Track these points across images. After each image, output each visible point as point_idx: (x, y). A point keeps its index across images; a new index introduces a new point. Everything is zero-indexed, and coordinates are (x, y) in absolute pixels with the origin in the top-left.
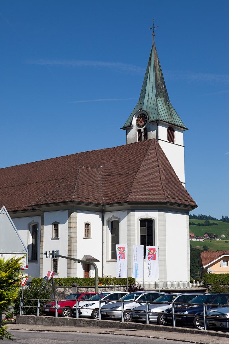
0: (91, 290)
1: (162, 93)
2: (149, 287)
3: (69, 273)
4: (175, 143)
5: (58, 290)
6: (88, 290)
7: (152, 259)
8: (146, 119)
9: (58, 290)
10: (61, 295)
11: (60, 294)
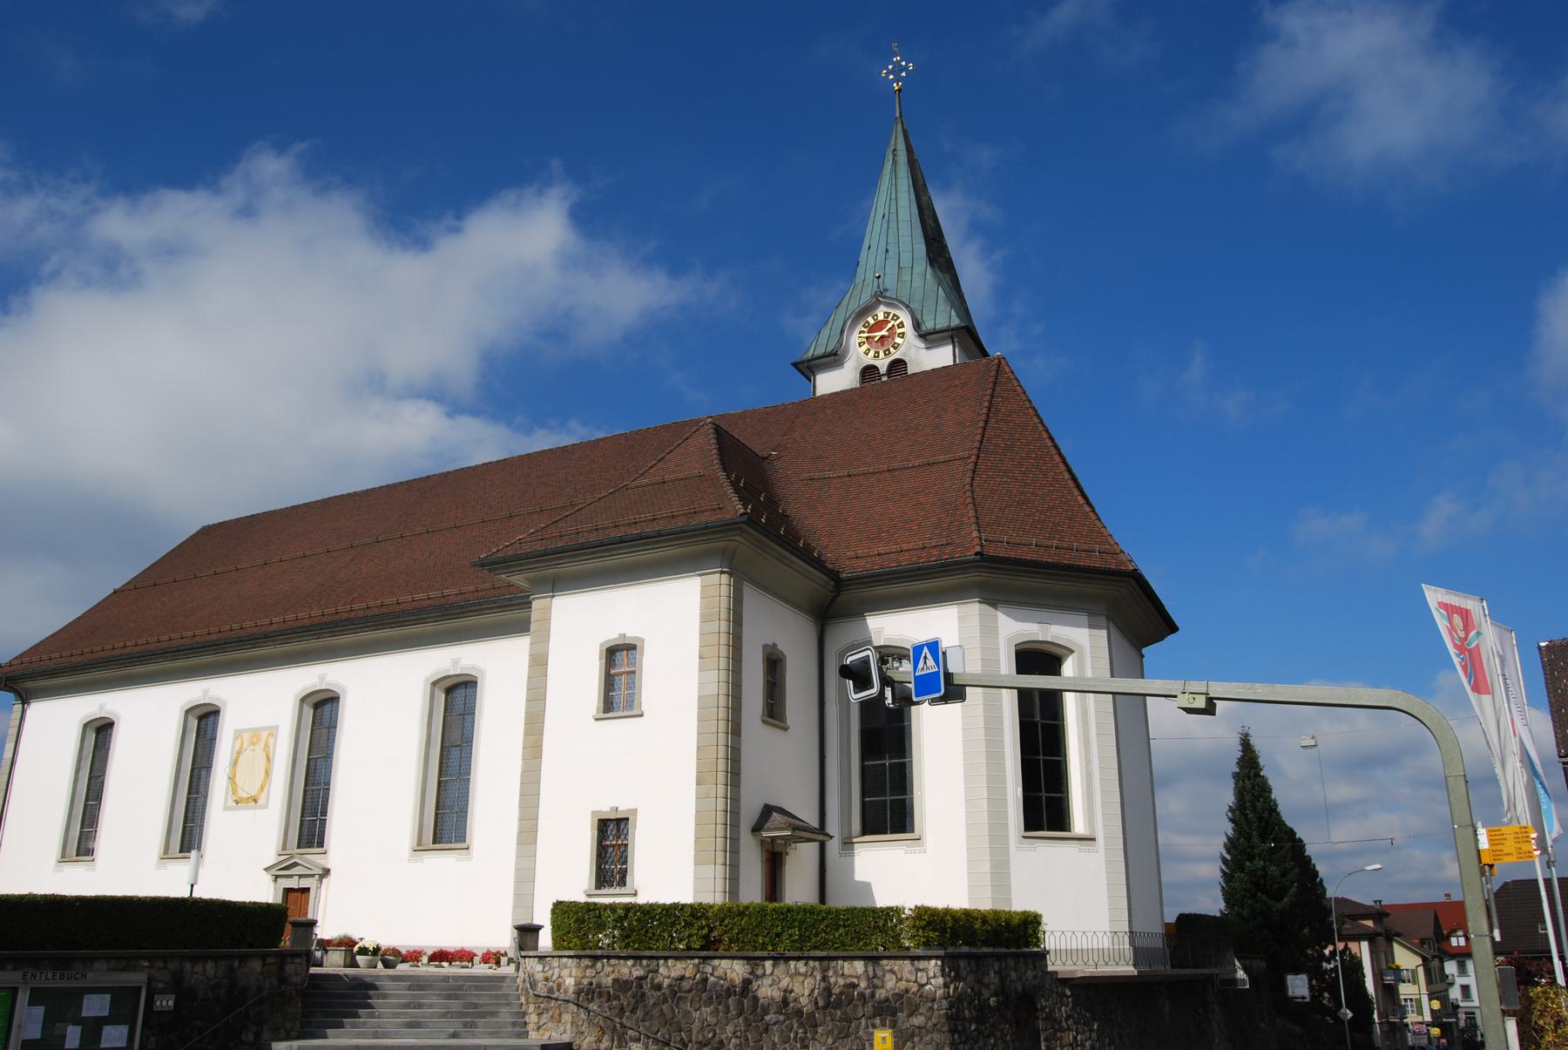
0: (892, 971)
6: (879, 973)
9: (714, 968)
11: (729, 992)
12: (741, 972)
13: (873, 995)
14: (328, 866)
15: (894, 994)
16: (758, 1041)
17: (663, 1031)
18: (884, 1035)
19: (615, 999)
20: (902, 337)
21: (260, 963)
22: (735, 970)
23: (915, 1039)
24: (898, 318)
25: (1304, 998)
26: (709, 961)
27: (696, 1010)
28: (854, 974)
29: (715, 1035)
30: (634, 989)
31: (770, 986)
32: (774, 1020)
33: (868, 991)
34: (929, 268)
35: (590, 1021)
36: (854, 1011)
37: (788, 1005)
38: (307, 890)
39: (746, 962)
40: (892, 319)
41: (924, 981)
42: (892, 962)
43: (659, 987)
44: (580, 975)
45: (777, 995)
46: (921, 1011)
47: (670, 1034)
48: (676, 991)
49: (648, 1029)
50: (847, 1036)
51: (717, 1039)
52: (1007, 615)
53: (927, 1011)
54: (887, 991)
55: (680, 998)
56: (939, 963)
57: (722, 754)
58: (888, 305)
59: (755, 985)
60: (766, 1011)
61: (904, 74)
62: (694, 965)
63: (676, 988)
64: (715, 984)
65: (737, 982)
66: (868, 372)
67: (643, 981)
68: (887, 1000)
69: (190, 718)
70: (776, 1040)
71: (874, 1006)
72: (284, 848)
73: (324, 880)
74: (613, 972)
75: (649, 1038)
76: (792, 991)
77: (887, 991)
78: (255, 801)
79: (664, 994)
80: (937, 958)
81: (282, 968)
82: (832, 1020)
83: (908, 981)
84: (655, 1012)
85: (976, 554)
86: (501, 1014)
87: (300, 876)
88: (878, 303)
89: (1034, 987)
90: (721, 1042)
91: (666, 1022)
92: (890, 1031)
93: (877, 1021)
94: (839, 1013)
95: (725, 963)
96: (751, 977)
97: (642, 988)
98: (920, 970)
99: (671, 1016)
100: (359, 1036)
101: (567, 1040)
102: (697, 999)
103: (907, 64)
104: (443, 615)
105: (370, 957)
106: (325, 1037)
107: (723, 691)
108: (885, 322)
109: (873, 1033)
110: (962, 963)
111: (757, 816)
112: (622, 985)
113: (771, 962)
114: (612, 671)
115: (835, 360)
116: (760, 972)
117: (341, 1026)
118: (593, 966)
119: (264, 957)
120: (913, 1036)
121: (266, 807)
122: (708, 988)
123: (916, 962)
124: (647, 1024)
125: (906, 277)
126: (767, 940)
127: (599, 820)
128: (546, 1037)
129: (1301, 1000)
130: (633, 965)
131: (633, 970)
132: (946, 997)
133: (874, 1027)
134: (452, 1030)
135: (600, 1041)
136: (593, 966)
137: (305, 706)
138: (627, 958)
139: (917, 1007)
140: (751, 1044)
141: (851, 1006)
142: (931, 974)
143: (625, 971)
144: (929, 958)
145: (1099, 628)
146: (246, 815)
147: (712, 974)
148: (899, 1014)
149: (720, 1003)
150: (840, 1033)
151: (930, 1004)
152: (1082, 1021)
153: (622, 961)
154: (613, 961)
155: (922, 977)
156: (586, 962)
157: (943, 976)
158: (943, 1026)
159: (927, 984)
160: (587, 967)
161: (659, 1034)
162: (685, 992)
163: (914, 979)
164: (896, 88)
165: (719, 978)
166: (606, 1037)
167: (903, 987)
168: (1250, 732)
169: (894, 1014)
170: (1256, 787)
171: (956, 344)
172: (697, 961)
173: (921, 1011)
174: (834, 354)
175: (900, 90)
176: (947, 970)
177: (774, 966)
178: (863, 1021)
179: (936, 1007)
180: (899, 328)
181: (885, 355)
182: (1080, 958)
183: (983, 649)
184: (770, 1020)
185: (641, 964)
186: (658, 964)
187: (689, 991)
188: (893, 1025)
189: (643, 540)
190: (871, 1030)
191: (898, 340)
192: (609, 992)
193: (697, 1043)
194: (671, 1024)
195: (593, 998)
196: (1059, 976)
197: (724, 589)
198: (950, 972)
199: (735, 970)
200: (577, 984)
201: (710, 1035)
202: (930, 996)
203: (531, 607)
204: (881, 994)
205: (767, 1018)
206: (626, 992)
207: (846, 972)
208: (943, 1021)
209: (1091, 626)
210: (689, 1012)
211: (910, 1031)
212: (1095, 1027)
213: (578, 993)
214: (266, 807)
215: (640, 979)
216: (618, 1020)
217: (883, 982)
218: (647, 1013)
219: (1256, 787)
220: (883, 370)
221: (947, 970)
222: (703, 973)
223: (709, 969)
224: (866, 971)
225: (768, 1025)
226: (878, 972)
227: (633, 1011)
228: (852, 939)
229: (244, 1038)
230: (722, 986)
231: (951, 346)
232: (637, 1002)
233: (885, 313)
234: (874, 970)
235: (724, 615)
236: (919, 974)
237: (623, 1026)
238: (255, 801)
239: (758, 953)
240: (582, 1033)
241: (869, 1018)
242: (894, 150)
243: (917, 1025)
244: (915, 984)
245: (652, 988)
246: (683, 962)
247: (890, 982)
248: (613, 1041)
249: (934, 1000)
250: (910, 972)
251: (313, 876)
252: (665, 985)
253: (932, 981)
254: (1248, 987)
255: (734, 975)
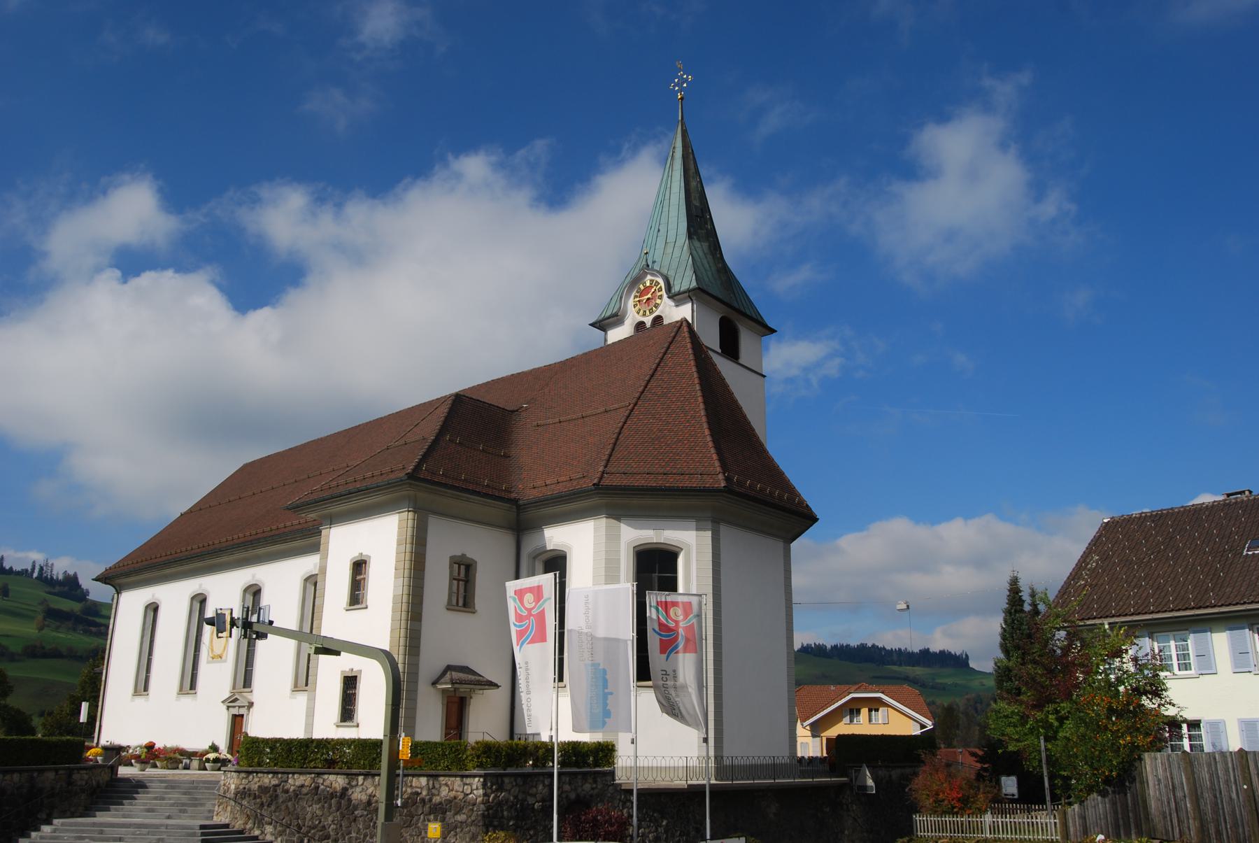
0: (446, 785)
1: (703, 231)
2: (663, 776)
3: (309, 725)
4: (741, 361)
5: (324, 780)
6: (437, 786)
7: (532, 642)
8: (659, 294)
9: (324, 780)
10: (333, 801)
11: (333, 795)
12: (341, 783)
13: (430, 800)
14: (253, 701)
15: (446, 800)
16: (348, 827)
17: (287, 818)
18: (434, 826)
19: (258, 798)
20: (661, 299)
21: (54, 773)
22: (338, 782)
23: (458, 830)
24: (659, 284)
25: (1013, 795)
26: (321, 776)
27: (309, 806)
28: (419, 786)
29: (320, 823)
30: (271, 792)
31: (360, 792)
32: (360, 814)
33: (428, 797)
34: (687, 240)
35: (242, 811)
36: (416, 810)
37: (371, 804)
38: (242, 716)
39: (345, 776)
40: (655, 285)
41: (469, 791)
42: (447, 778)
43: (287, 791)
44: (239, 783)
45: (364, 798)
46: (464, 812)
47: (291, 821)
48: (297, 794)
49: (277, 817)
50: (409, 826)
51: (321, 824)
52: (629, 525)
53: (468, 812)
54: (441, 798)
55: (301, 798)
56: (482, 780)
57: (403, 634)
58: (652, 275)
59: (350, 792)
60: (356, 808)
61: (685, 85)
62: (311, 778)
63: (298, 792)
64: (323, 790)
65: (338, 789)
66: (640, 326)
67: (277, 788)
68: (440, 803)
69: (195, 602)
70: (361, 827)
71: (430, 807)
72: (234, 687)
73: (251, 709)
74: (259, 781)
75: (277, 822)
76: (375, 796)
77: (441, 798)
78: (221, 657)
79: (289, 796)
80: (480, 776)
81: (70, 776)
82: (400, 815)
83: (457, 791)
84: (283, 807)
85: (594, 485)
86: (207, 805)
87: (239, 707)
88: (646, 274)
89: (591, 796)
90: (324, 827)
91: (289, 813)
92: (440, 824)
93: (432, 817)
94: (405, 811)
95: (332, 777)
96: (348, 786)
97: (276, 791)
98: (467, 784)
99: (293, 809)
100: (124, 816)
101: (227, 822)
102: (311, 799)
103: (687, 77)
104: (303, 536)
105: (212, 764)
106: (95, 816)
107: (406, 592)
108: (651, 287)
109: (427, 825)
110: (506, 780)
111: (440, 674)
112: (264, 789)
113: (363, 777)
114: (358, 578)
115: (618, 320)
116: (354, 783)
117: (109, 810)
118: (247, 778)
119: (56, 771)
120: (456, 827)
121: (225, 661)
122: (319, 792)
123: (464, 779)
124: (277, 814)
125: (669, 250)
126: (366, 762)
127: (345, 677)
128: (219, 820)
129: (1011, 797)
130: (273, 777)
131: (272, 780)
132: (483, 803)
133: (429, 821)
134: (168, 814)
135: (246, 823)
136: (247, 778)
137: (308, 584)
138: (268, 773)
139: (461, 809)
140: (344, 829)
141: (414, 807)
142: (474, 787)
143: (267, 781)
144: (474, 776)
145: (704, 529)
146: (216, 666)
147: (322, 784)
148: (448, 813)
149: (326, 802)
150: (404, 824)
151: (471, 807)
152: (648, 819)
153: (265, 775)
154: (259, 775)
155: (467, 789)
156: (243, 775)
157: (483, 789)
158: (479, 822)
159: (471, 793)
160: (243, 778)
161: (284, 820)
162: (304, 795)
163: (461, 790)
164: (679, 97)
165: (326, 786)
166: (250, 821)
167: (452, 796)
168: (1019, 576)
169: (444, 812)
170: (1016, 622)
171: (695, 301)
172: (313, 775)
173: (464, 812)
174: (616, 315)
175: (682, 99)
176: (489, 784)
177: (364, 780)
178: (422, 817)
179: (475, 809)
180: (659, 291)
181: (650, 313)
182: (668, 775)
183: (607, 551)
184: (358, 814)
185: (277, 778)
186: (288, 777)
187: (307, 794)
188: (443, 820)
189: (366, 491)
190: (426, 823)
191: (658, 301)
192: (255, 794)
193: (308, 827)
194: (292, 815)
195: (245, 797)
196: (623, 788)
197: (410, 522)
198: (492, 786)
199: (338, 782)
200: (237, 788)
201: (317, 822)
202: (472, 802)
203: (321, 535)
204: (436, 799)
205: (356, 813)
206: (266, 794)
207: (414, 785)
208: (479, 818)
209: (698, 529)
210: (305, 807)
211: (454, 825)
212: (664, 823)
213: (236, 794)
214: (225, 661)
215: (275, 786)
216: (259, 811)
217: (439, 791)
218: (278, 807)
219: (1016, 622)
220: (648, 325)
221: (489, 784)
222: (317, 783)
223: (321, 781)
224: (428, 784)
225: (356, 817)
226: (436, 785)
227: (269, 806)
228: (427, 762)
229: (39, 816)
230: (328, 792)
231: (690, 304)
232: (272, 800)
233: (650, 281)
234: (433, 783)
235: (409, 540)
236: (466, 787)
237: (261, 815)
238: (221, 657)
239: (354, 771)
240: (236, 818)
241: (426, 815)
242: (674, 148)
243: (460, 820)
244: (462, 794)
245: (282, 792)
246: (304, 776)
247: (444, 792)
248: (255, 824)
249: (474, 805)
250: (459, 786)
251: (244, 707)
252: (291, 790)
253: (475, 792)
254: (874, 792)
255: (337, 785)
